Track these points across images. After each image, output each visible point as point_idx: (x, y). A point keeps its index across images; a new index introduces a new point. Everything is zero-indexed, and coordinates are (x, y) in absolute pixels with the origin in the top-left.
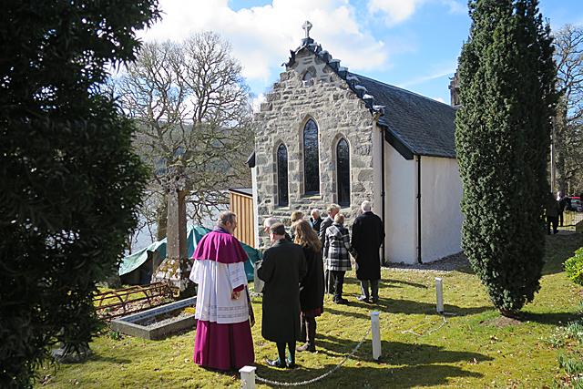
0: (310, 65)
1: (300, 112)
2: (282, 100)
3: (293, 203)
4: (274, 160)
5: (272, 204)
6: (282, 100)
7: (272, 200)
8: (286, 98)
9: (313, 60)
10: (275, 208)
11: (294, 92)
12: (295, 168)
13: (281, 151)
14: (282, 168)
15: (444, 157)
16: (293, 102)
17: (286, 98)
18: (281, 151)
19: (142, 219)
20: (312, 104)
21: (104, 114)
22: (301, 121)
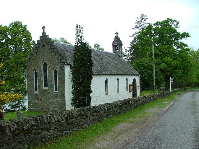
15: (103, 75)
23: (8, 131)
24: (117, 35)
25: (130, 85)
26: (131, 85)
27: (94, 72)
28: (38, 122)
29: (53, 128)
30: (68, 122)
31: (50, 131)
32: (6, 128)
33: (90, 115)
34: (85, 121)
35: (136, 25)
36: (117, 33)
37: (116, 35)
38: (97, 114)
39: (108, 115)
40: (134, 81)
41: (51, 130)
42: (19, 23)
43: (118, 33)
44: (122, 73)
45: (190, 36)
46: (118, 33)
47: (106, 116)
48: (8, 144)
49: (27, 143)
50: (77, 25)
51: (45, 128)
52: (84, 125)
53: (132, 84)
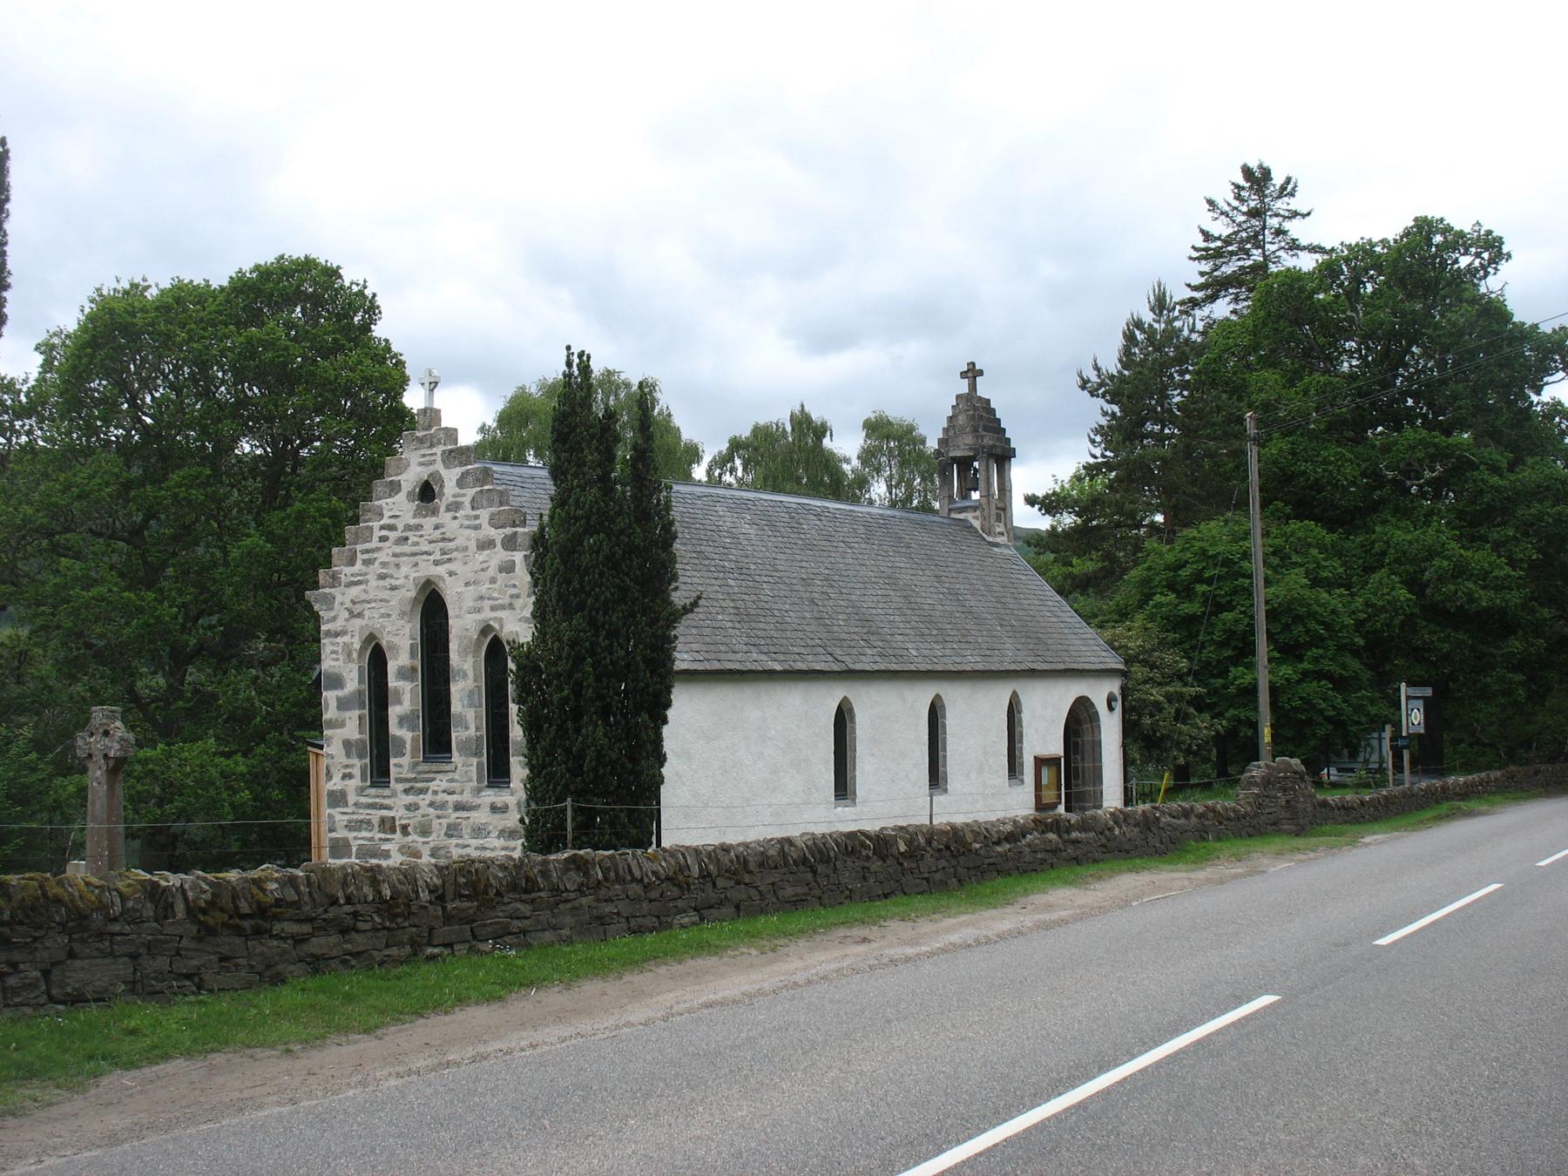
0: (432, 469)
1: (409, 577)
2: (374, 544)
3: (399, 780)
4: (361, 681)
5: (355, 782)
6: (374, 544)
7: (357, 772)
8: (383, 539)
9: (439, 458)
10: (360, 791)
11: (400, 527)
12: (406, 698)
13: (377, 659)
14: (378, 696)
15: (769, 675)
16: (398, 549)
17: (383, 539)
18: (377, 659)
19: (1335, 536)
20: (437, 556)
21: (328, 286)
22: (413, 594)
23: (180, 908)
24: (973, 387)
25: (1040, 762)
26: (1052, 762)
27: (683, 659)
28: (298, 892)
29: (368, 926)
30: (444, 908)
31: (354, 934)
32: (173, 896)
33: (579, 890)
34: (545, 915)
35: (1206, 266)
36: (972, 373)
37: (963, 386)
38: (625, 891)
39: (711, 907)
40: (1080, 721)
41: (357, 931)
42: (867, 420)
43: (981, 373)
44: (973, 662)
45: (339, 267)
46: (981, 373)
47: (695, 909)
48: (178, 954)
49: (252, 967)
50: (568, 348)
51: (332, 920)
52: (540, 934)
53: (1056, 748)
